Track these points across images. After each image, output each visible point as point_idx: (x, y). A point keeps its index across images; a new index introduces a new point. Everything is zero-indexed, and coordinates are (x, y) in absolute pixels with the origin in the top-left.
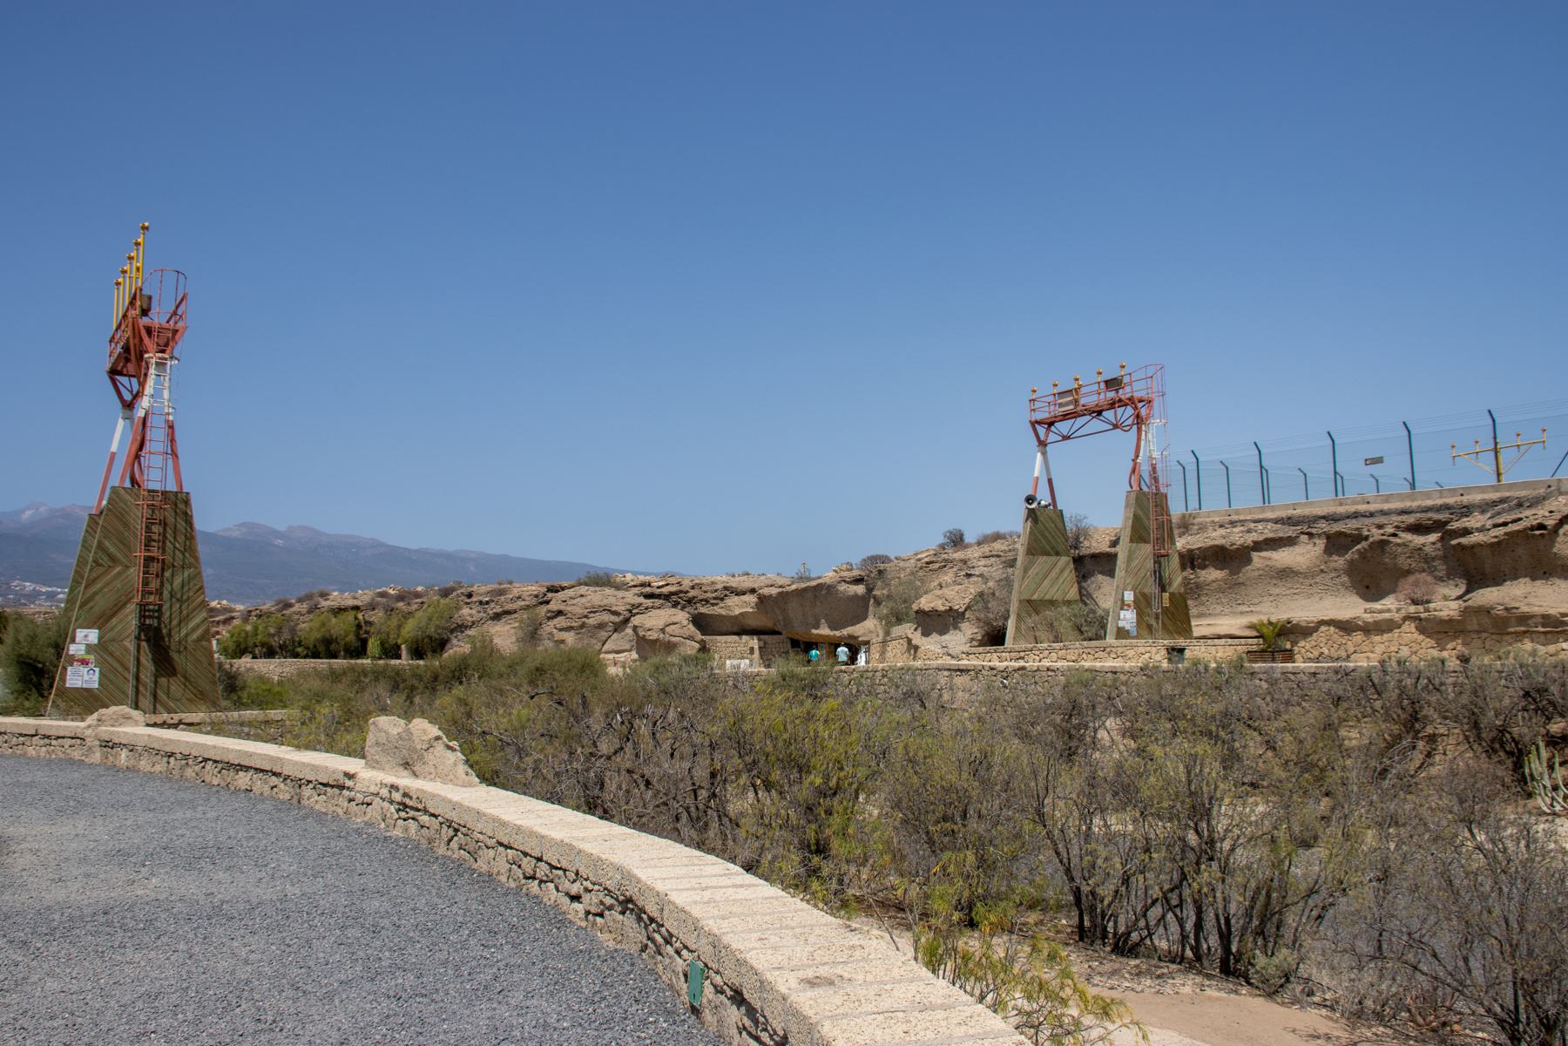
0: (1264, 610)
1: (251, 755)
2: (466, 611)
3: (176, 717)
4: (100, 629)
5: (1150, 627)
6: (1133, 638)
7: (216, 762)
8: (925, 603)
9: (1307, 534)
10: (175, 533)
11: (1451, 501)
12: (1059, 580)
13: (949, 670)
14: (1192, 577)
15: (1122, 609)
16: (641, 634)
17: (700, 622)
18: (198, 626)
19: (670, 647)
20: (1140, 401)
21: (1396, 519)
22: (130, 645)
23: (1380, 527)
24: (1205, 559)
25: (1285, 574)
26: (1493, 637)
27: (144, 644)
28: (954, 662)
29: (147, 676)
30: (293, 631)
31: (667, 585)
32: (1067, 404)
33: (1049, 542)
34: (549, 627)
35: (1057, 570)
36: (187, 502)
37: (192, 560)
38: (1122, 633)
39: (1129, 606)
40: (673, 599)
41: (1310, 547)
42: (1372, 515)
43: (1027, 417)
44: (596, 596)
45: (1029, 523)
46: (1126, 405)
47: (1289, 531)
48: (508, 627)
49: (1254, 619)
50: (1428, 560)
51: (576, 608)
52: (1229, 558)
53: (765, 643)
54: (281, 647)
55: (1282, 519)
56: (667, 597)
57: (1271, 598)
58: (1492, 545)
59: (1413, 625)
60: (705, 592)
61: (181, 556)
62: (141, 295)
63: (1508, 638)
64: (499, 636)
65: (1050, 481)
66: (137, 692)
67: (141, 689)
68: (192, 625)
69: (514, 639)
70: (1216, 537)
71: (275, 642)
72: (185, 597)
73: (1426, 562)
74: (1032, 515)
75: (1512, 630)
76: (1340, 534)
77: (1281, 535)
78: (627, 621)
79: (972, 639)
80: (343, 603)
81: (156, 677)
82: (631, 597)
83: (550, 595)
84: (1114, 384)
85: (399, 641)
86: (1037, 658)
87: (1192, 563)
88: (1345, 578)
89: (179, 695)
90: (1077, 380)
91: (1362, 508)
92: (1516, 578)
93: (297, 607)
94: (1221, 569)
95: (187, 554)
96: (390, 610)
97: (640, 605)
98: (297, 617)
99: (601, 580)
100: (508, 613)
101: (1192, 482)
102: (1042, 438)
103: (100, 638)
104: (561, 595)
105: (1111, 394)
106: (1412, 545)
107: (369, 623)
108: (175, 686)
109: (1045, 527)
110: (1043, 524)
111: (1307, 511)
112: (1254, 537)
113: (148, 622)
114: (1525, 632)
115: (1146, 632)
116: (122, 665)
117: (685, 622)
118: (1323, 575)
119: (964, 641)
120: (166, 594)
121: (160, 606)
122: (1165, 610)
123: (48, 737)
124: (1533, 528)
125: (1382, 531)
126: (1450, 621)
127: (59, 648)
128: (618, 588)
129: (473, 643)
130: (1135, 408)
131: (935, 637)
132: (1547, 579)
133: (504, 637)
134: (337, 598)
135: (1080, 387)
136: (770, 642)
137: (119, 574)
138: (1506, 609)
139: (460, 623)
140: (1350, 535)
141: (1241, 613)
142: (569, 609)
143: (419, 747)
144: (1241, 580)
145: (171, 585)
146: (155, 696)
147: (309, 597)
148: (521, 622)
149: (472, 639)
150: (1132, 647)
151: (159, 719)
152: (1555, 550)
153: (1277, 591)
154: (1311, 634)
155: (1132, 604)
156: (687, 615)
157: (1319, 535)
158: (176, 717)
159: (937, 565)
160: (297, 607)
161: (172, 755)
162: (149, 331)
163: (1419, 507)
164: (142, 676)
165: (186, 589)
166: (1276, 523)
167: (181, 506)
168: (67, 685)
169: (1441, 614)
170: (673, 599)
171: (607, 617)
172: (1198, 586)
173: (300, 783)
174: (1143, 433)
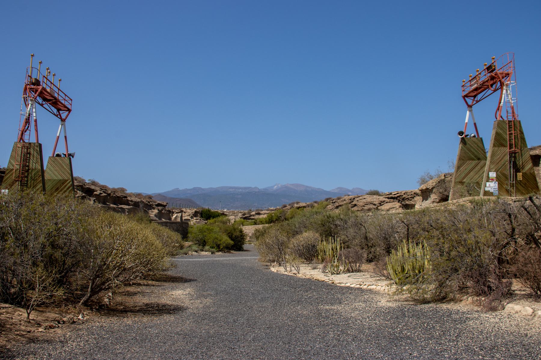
10: (33, 157)
15: (487, 181)
31: (398, 193)
33: (473, 154)
39: (492, 180)
45: (461, 145)
60: (408, 195)
61: (35, 165)
65: (475, 124)
72: (35, 179)
74: (463, 141)
99: (376, 193)
100: (341, 206)
109: (472, 147)
142: (358, 203)
145: (31, 175)
155: (495, 179)
165: (36, 176)
171: (371, 206)
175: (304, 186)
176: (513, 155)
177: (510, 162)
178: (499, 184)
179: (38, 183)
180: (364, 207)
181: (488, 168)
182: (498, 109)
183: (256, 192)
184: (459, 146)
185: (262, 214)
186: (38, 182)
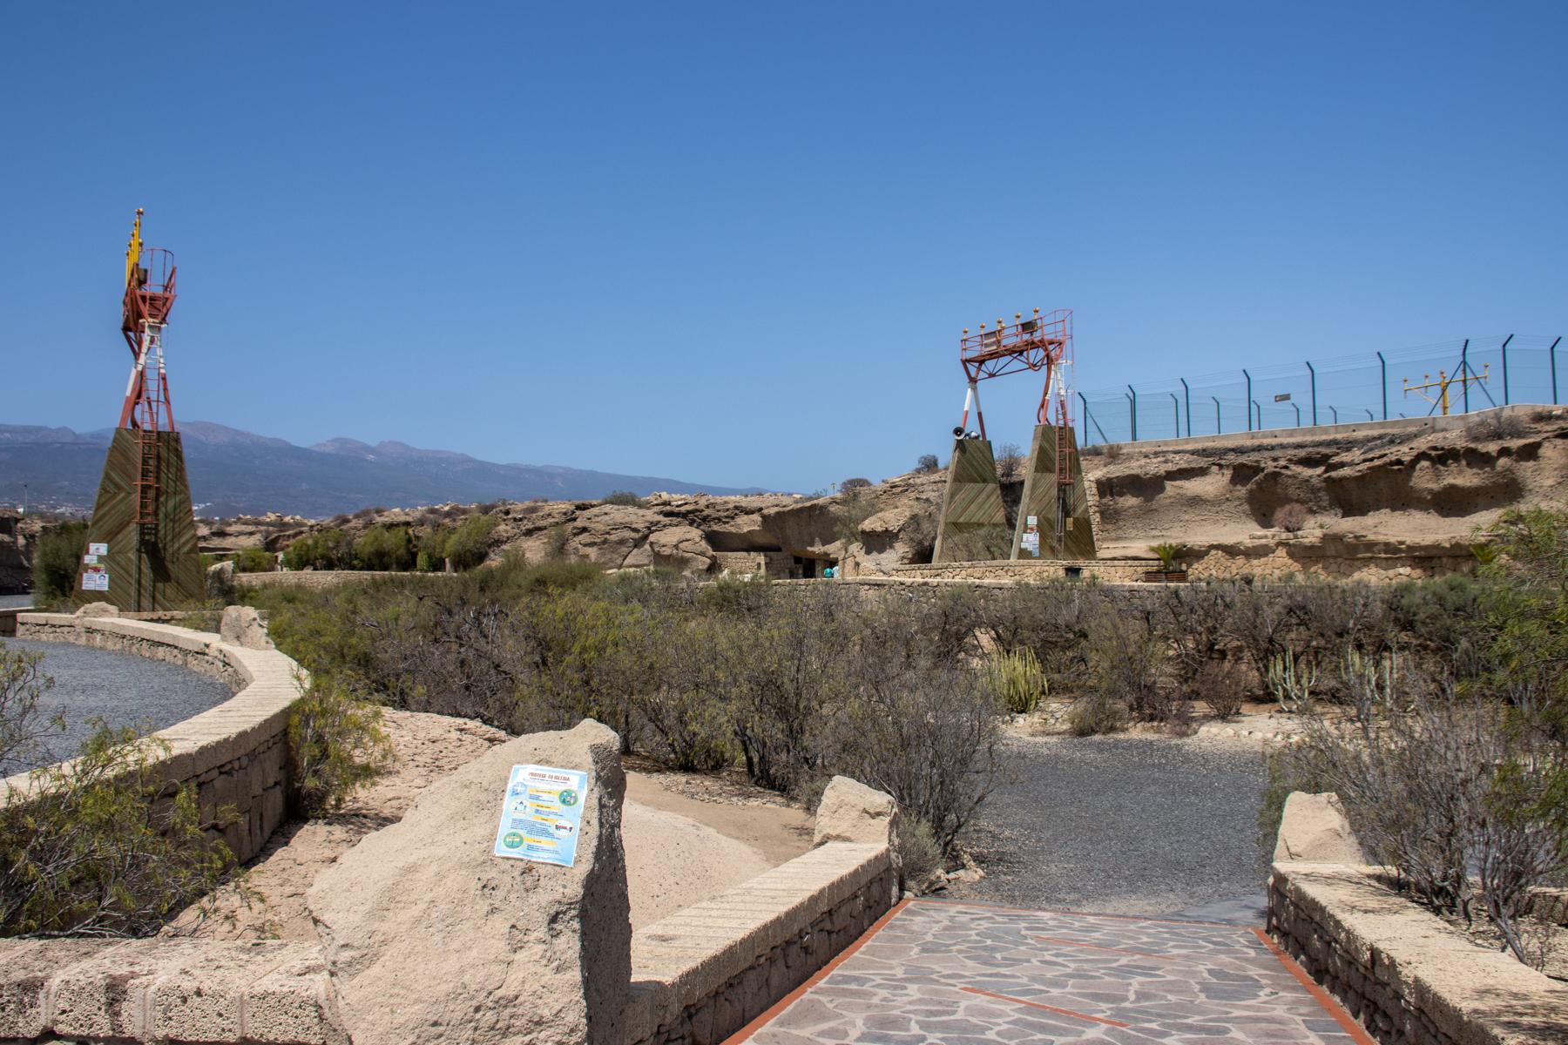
0: (1174, 535)
1: (164, 634)
2: (502, 527)
3: (169, 614)
4: (108, 543)
5: (1052, 549)
6: (1036, 558)
7: (148, 640)
8: (868, 525)
9: (1219, 465)
11: (1339, 436)
12: (990, 507)
13: (869, 585)
14: (1111, 503)
15: (1025, 532)
16: (656, 549)
17: (715, 540)
18: (188, 541)
19: (683, 562)
20: (1051, 343)
21: (1291, 452)
22: (133, 556)
23: (1275, 460)
24: (1122, 487)
25: (1195, 502)
26: (1347, 562)
27: (144, 556)
28: (885, 578)
29: (147, 581)
30: (350, 544)
31: (686, 504)
32: (991, 345)
33: (976, 470)
34: (575, 542)
35: (984, 495)
36: (177, 440)
37: (182, 487)
38: (1024, 554)
39: (1032, 529)
40: (689, 517)
41: (1219, 477)
42: (1273, 448)
43: (957, 355)
44: (619, 514)
45: (957, 453)
46: (1038, 347)
47: (1202, 462)
48: (538, 543)
49: (1155, 544)
50: (1314, 490)
51: (599, 525)
52: (1146, 486)
53: (771, 559)
54: (339, 559)
55: (1198, 450)
56: (684, 515)
57: (1181, 524)
58: (1356, 478)
59: (1285, 550)
60: (718, 511)
62: (138, 269)
63: (1358, 563)
64: (531, 551)
65: (980, 414)
66: (139, 594)
67: (143, 591)
68: (183, 540)
69: (543, 554)
70: (1134, 467)
71: (334, 555)
72: (177, 518)
73: (1313, 493)
74: (960, 445)
75: (1360, 556)
76: (1243, 466)
77: (1194, 465)
78: (646, 537)
79: (903, 558)
80: (396, 519)
81: (154, 582)
82: (651, 515)
83: (578, 513)
84: (1028, 327)
85: (444, 555)
86: (951, 575)
87: (1111, 490)
88: (1246, 507)
89: (173, 597)
90: (1000, 322)
91: (1267, 441)
92: (1378, 509)
93: (354, 523)
94: (1137, 497)
95: (178, 483)
96: (437, 526)
97: (659, 522)
98: (353, 532)
100: (539, 529)
101: (1182, 412)
102: (973, 375)
103: (109, 551)
104: (587, 513)
105: (1026, 337)
106: (1300, 477)
107: (418, 538)
108: (170, 590)
109: (974, 457)
110: (970, 453)
111: (1219, 444)
112: (1170, 467)
113: (147, 538)
114: (1371, 558)
115: (1049, 553)
116: (128, 573)
117: (698, 539)
118: (1228, 503)
119: (896, 559)
120: (161, 516)
121: (157, 525)
122: (1068, 534)
123: (53, 626)
124: (1392, 463)
125: (1275, 464)
126: (1312, 547)
127: (79, 558)
128: (640, 506)
129: (507, 557)
130: (1046, 350)
131: (875, 554)
132: (1404, 510)
133: (534, 551)
134: (396, 514)
135: (1003, 328)
136: (775, 558)
137: (124, 498)
138: (1356, 537)
139: (496, 538)
140: (1251, 467)
141: (1154, 537)
142: (593, 526)
143: (243, 625)
144: (1154, 507)
146: (154, 598)
147: (366, 513)
148: (550, 537)
149: (506, 553)
150: (1030, 566)
151: (155, 616)
152: (1411, 484)
153: (1187, 517)
154: (1203, 557)
156: (701, 533)
157: (1228, 466)
158: (169, 614)
159: (900, 489)
160: (354, 523)
161: (124, 637)
162: (144, 298)
163: (1312, 442)
164: (143, 581)
166: (1193, 454)
167: (173, 443)
168: (84, 588)
169: (1306, 540)
170: (689, 517)
171: (628, 534)
172: (1117, 512)
173: (186, 652)
174: (1053, 373)
175: (226, 429)
176: (1063, 488)
177: (1059, 499)
178: (1040, 537)
179: (185, 527)
180: (607, 536)
181: (1025, 509)
182: (1042, 406)
183: (63, 444)
184: (951, 454)
185: (231, 535)
186: (184, 524)
